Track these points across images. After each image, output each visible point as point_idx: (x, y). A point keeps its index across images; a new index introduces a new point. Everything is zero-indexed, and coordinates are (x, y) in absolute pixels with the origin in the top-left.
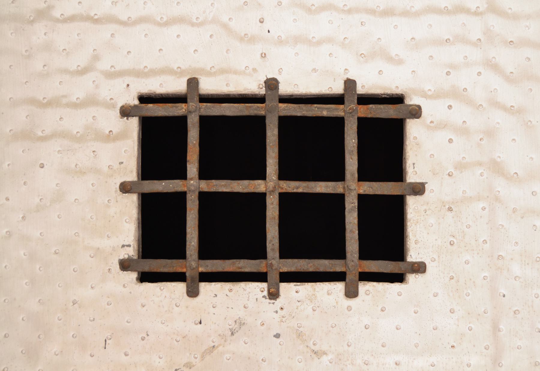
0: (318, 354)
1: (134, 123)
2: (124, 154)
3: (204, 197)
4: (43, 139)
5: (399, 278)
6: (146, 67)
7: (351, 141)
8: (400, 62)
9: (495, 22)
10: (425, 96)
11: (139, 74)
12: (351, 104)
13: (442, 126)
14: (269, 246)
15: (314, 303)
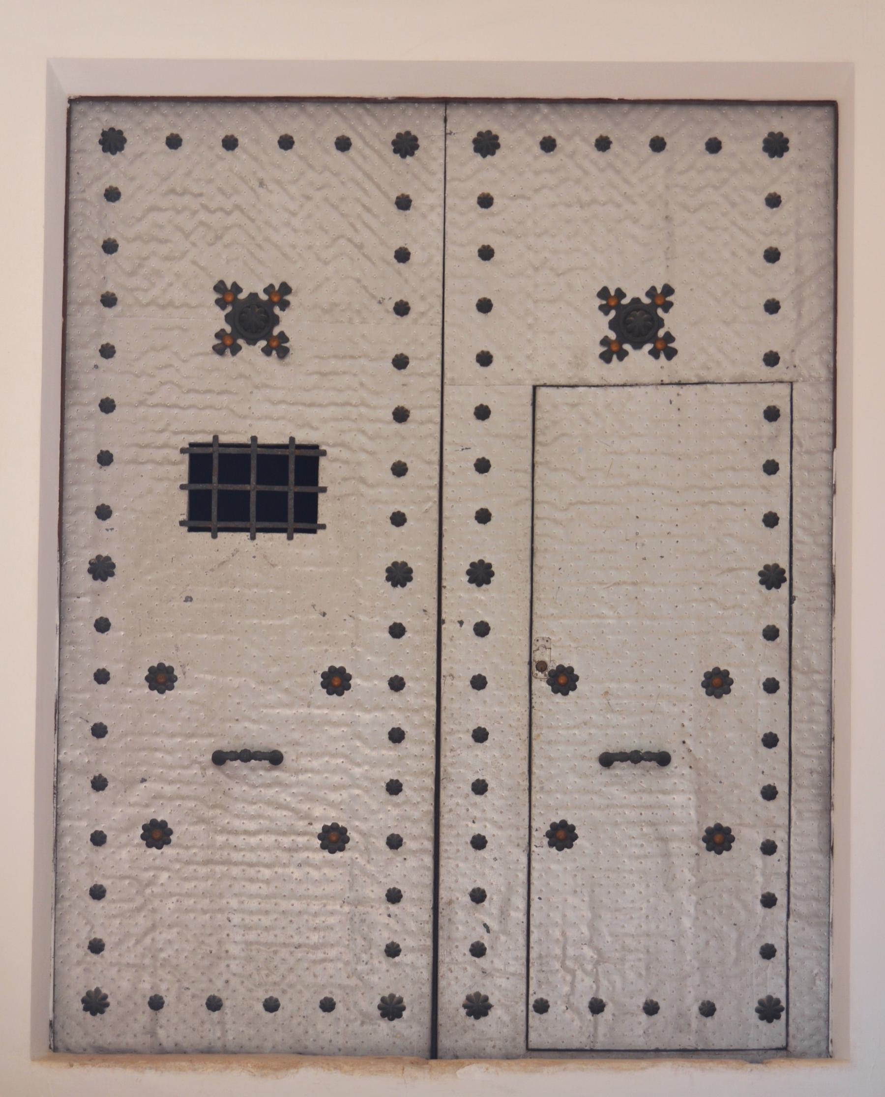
0: (273, 565)
1: (186, 457)
2: (182, 471)
3: (221, 493)
4: (142, 463)
5: (314, 531)
6: (457, 913)
7: (292, 466)
8: (317, 429)
9: (363, 410)
10: (328, 445)
11: (189, 433)
12: (292, 449)
13: (336, 460)
14: (251, 515)
15: (272, 543)
